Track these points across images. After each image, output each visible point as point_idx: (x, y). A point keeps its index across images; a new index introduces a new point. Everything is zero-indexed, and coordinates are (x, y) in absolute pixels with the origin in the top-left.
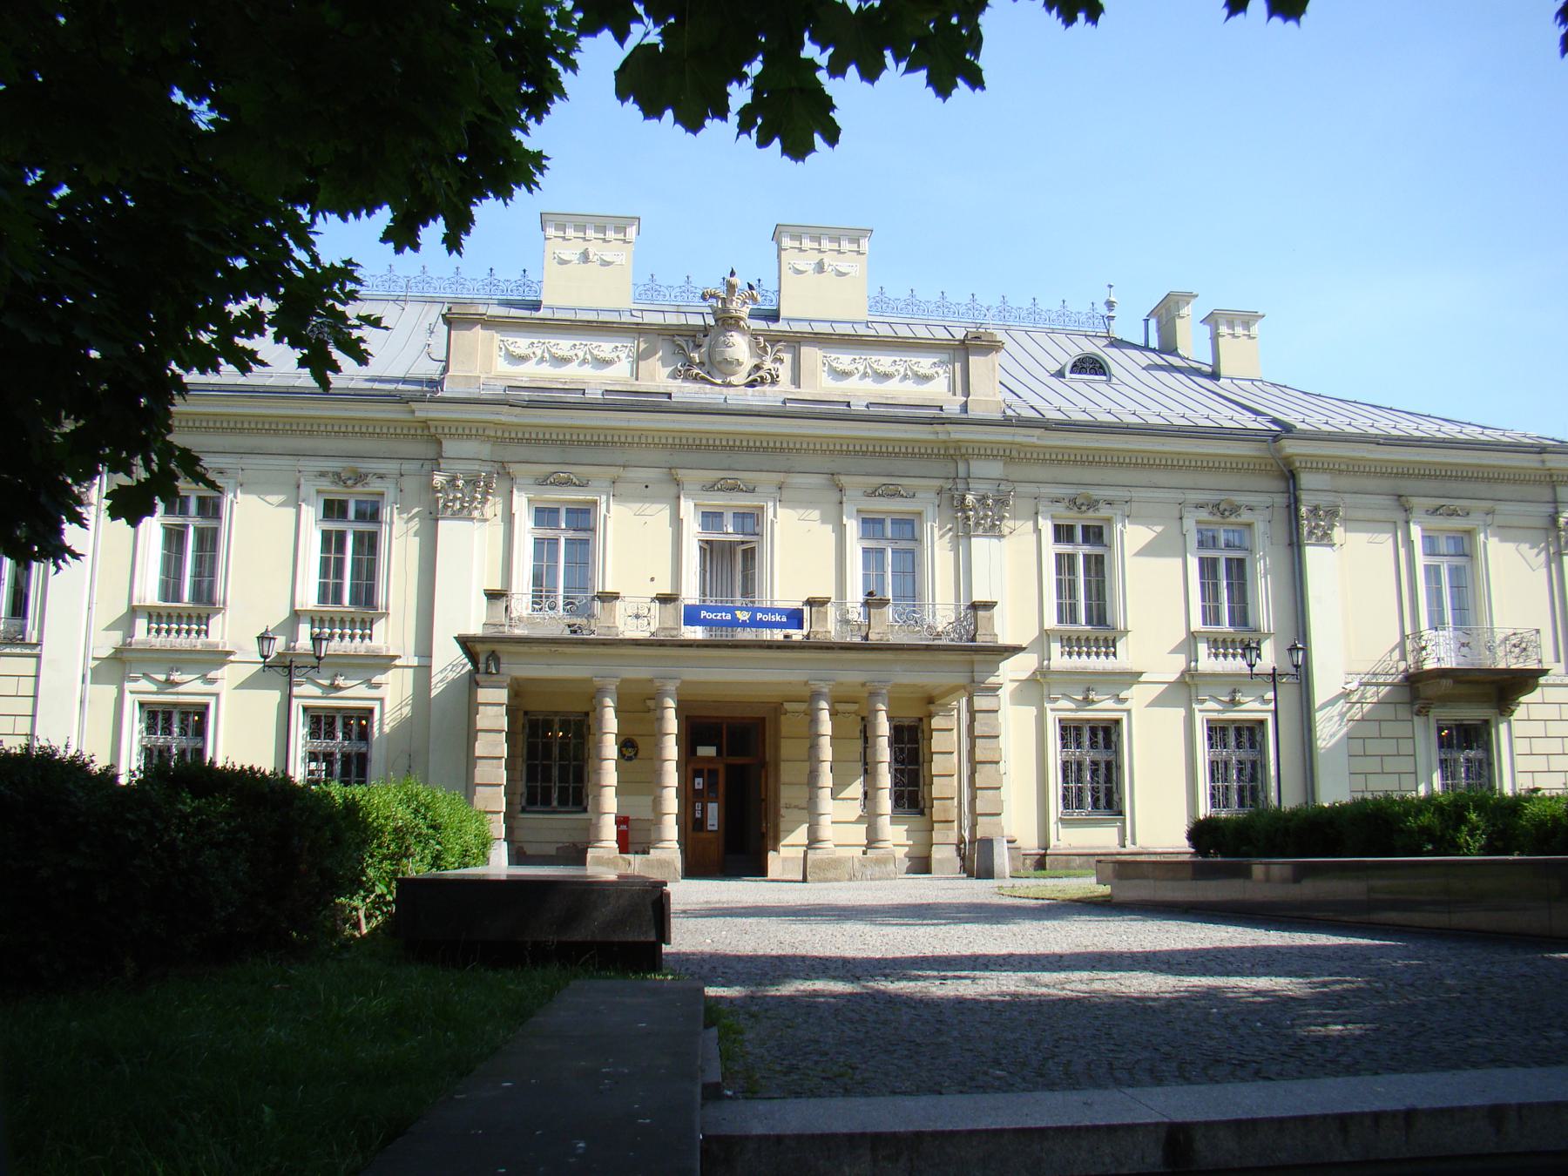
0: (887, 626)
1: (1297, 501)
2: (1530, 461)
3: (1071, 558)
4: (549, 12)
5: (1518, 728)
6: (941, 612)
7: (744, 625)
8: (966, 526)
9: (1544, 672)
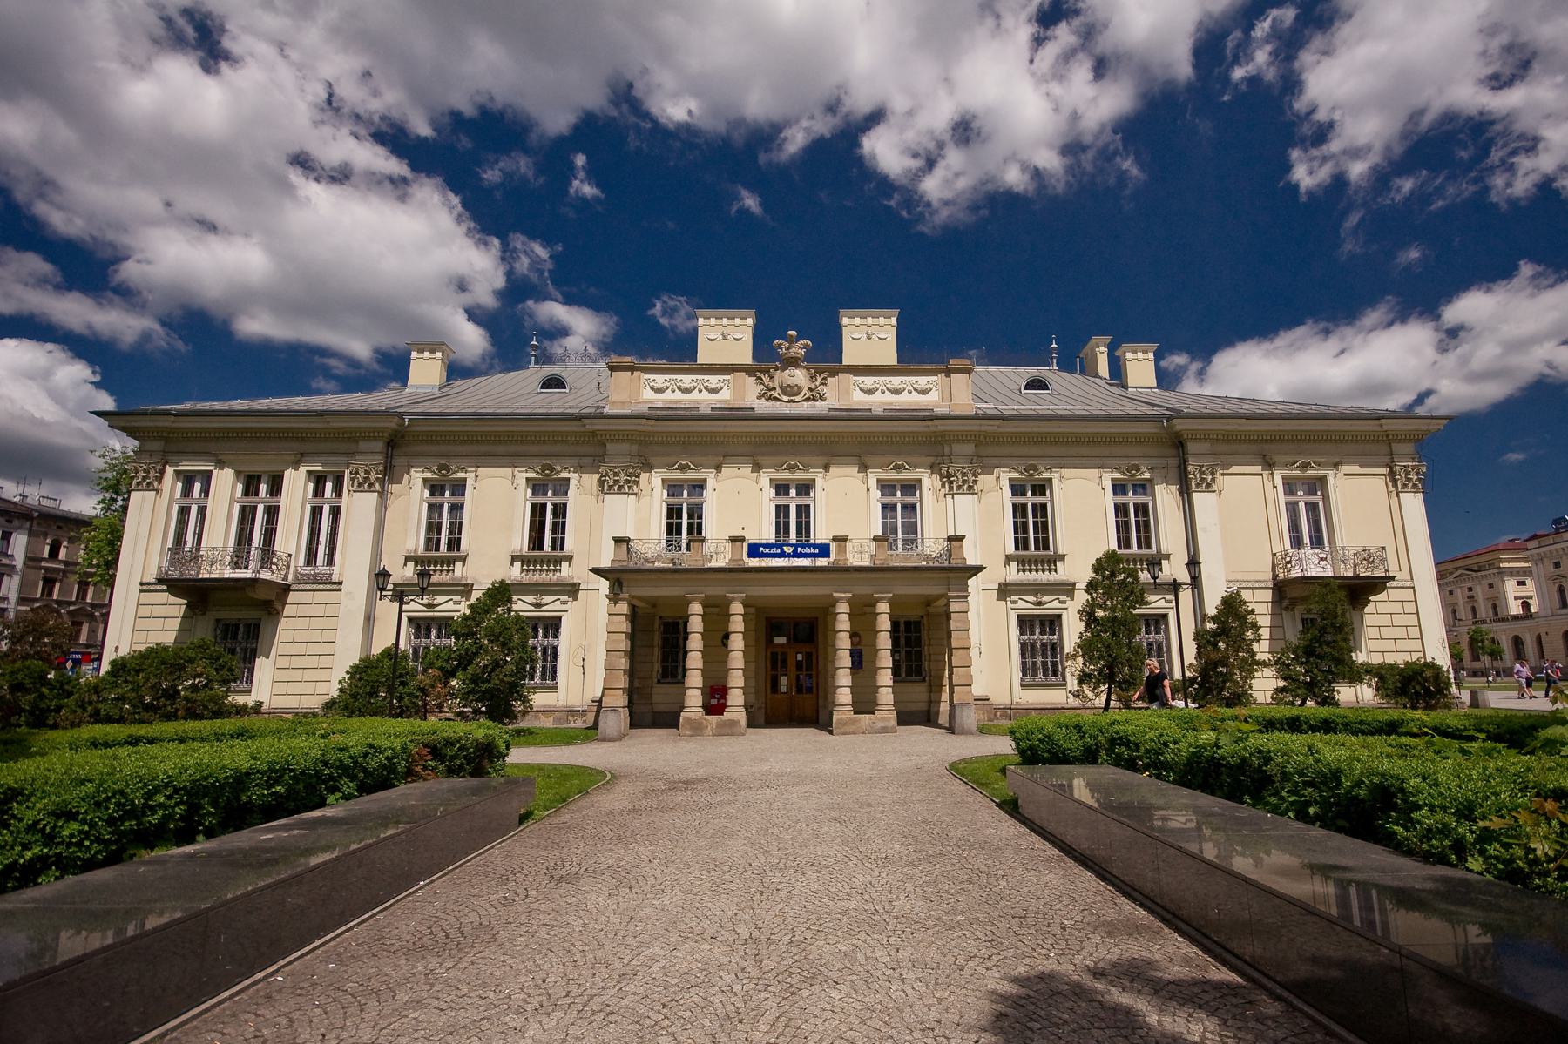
0: (898, 557)
1: (1185, 461)
2: (1371, 426)
3: (1024, 506)
4: (588, 190)
5: (1368, 620)
6: (931, 543)
7: (789, 556)
8: (951, 488)
9: (1393, 578)
